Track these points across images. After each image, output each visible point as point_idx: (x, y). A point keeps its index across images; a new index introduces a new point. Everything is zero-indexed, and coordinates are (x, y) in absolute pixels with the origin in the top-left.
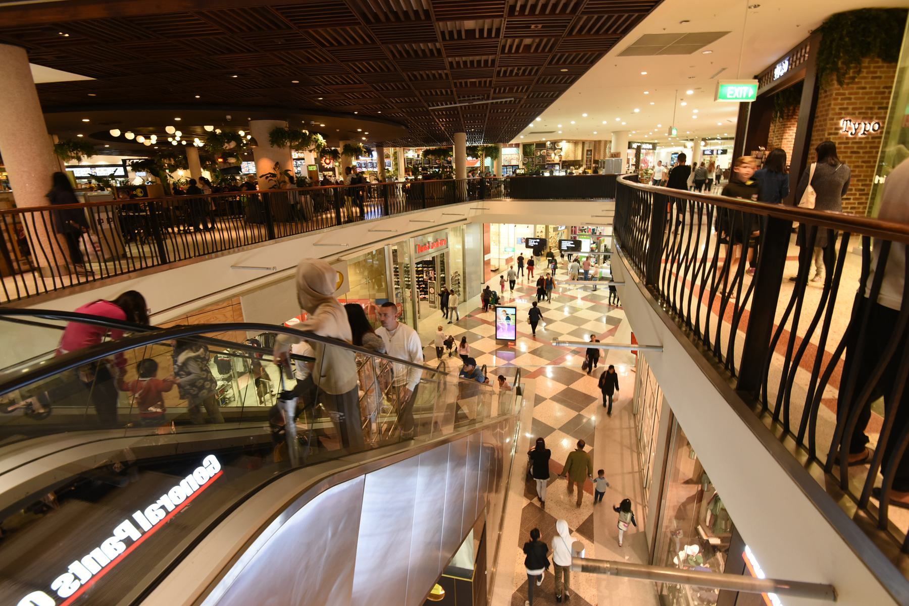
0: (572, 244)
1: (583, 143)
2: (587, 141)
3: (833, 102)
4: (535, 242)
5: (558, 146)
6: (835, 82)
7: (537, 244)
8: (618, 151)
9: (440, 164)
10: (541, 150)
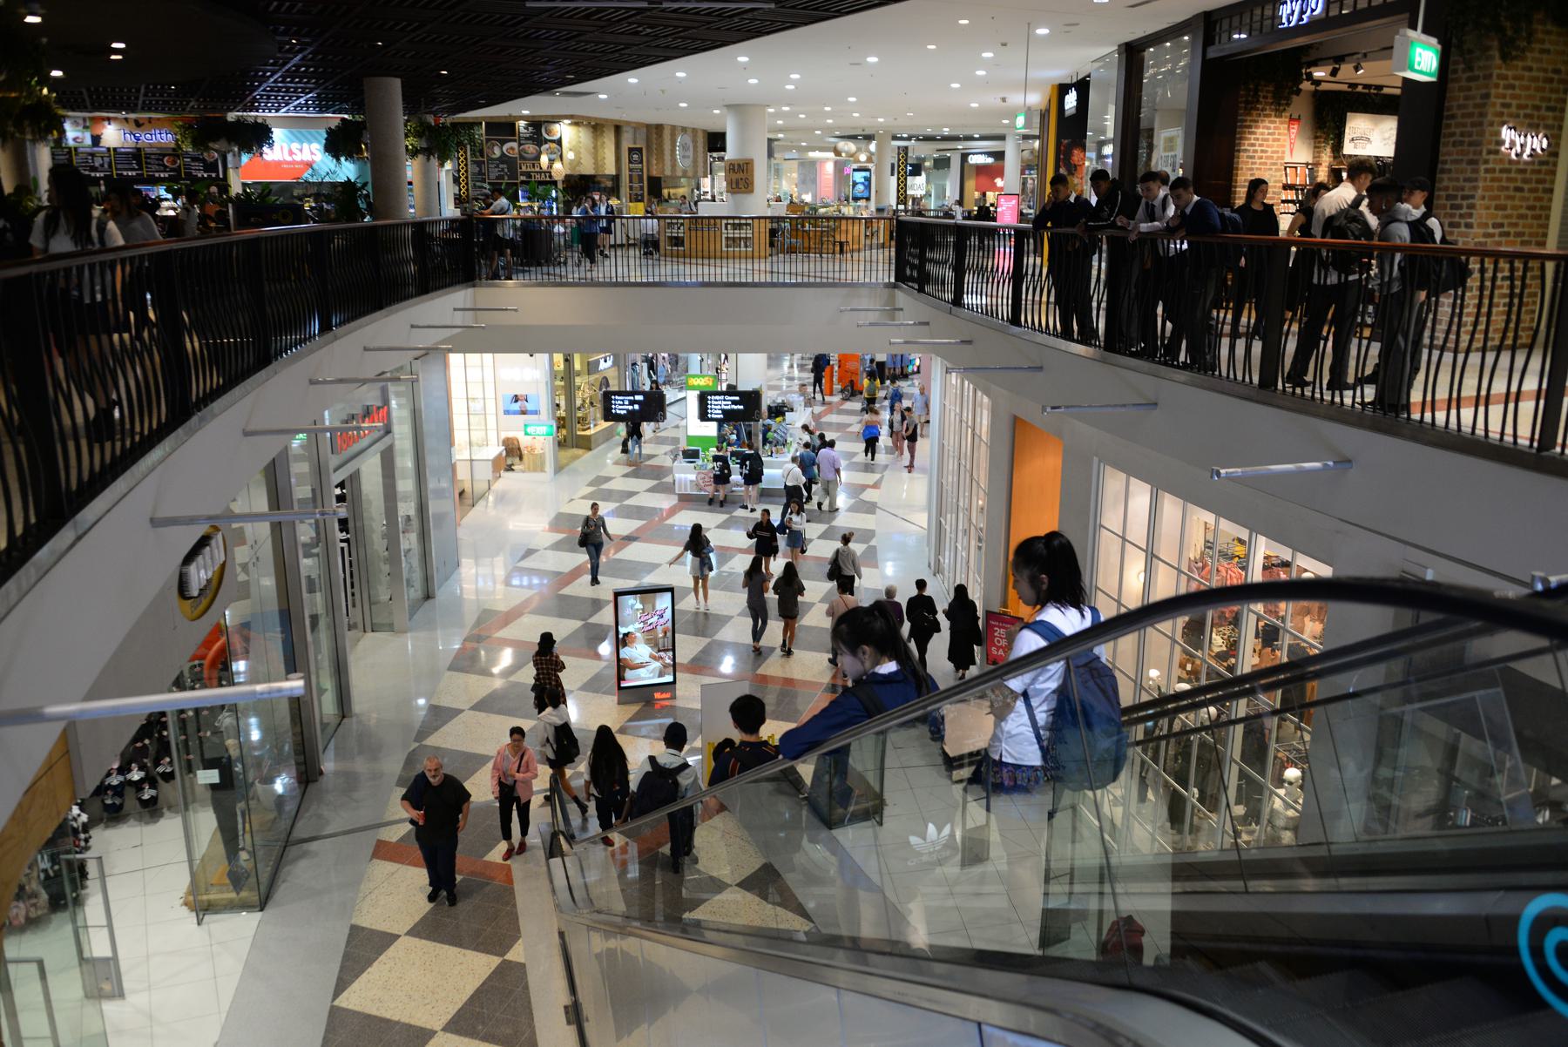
0: (734, 403)
1: (618, 129)
2: (628, 123)
3: (1493, 91)
4: (632, 403)
5: (548, 132)
6: (1496, 54)
7: (636, 407)
8: (747, 156)
9: (178, 170)
10: (503, 142)
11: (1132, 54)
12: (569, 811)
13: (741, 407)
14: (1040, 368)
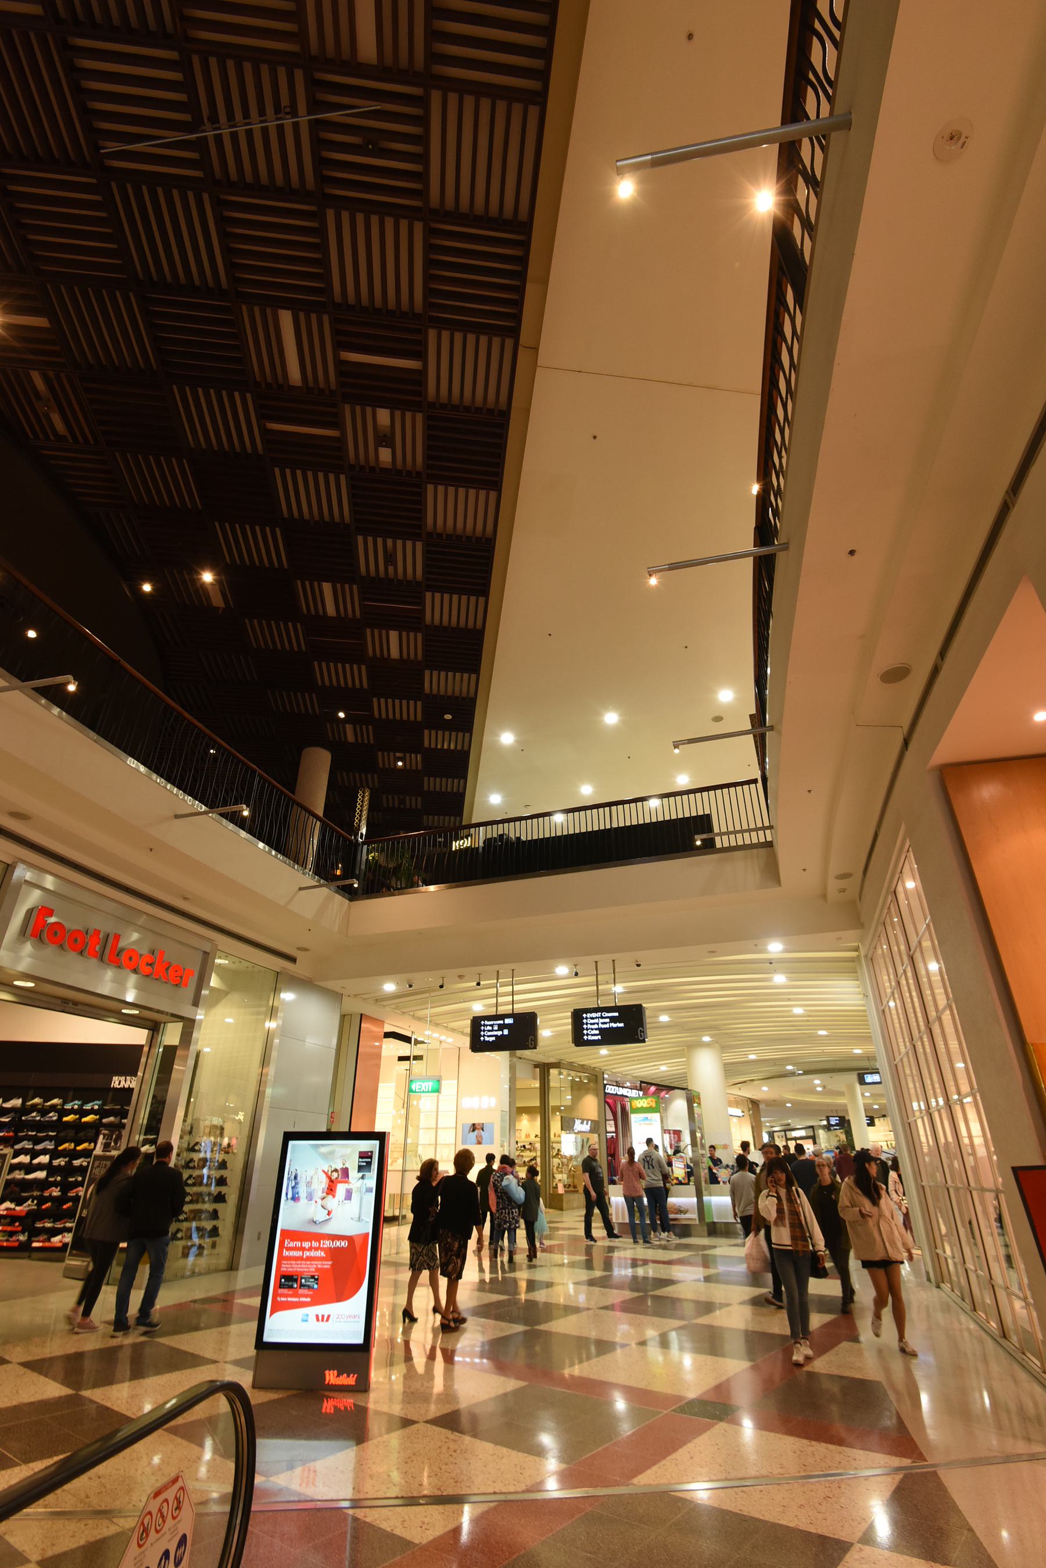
0: (613, 1020)
4: (501, 1027)
11: (381, 1137)
12: (468, 340)
13: (622, 1025)
14: (259, 1238)
